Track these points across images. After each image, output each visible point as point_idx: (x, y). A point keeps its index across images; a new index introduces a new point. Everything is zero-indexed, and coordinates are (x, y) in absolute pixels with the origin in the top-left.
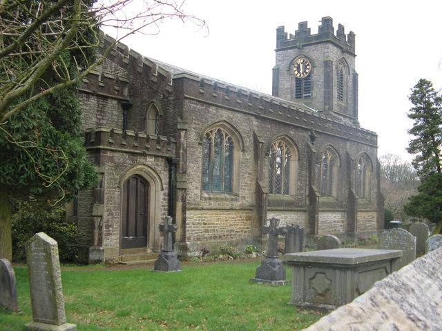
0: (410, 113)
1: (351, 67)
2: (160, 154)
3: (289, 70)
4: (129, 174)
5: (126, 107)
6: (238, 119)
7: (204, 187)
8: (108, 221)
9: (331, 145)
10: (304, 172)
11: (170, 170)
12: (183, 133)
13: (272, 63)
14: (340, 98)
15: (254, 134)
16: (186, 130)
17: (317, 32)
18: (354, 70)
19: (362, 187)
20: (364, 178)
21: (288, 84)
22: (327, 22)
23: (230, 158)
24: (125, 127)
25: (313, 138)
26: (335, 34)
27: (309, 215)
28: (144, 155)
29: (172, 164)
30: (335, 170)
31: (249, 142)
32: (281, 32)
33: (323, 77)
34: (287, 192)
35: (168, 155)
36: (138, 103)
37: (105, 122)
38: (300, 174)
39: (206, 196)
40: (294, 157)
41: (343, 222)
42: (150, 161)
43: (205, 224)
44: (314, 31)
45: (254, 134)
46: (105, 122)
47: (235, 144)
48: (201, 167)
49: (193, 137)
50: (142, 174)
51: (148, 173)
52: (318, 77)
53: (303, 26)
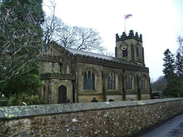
0: (164, 58)
1: (141, 46)
2: (70, 79)
3: (120, 48)
4: (60, 85)
5: (61, 64)
6: (95, 66)
7: (85, 88)
8: (53, 99)
9: (130, 73)
10: (121, 82)
11: (73, 84)
12: (77, 72)
13: (115, 46)
14: (138, 56)
15: (102, 71)
16: (78, 71)
17: (128, 35)
18: (142, 47)
19: (144, 86)
20: (145, 83)
21: (120, 52)
22: (131, 32)
23: (94, 79)
24: (61, 71)
25: (123, 71)
26: (135, 35)
27: (123, 96)
28: (65, 79)
29: (73, 81)
30: (133, 81)
31: (100, 74)
32: (117, 35)
33: (131, 50)
34: (115, 89)
35: (72, 79)
36: (64, 63)
37: (54, 69)
38: (119, 83)
39: (85, 91)
40: (117, 77)
41: (136, 98)
42: (66, 81)
43: (85, 100)
44: (128, 35)
45: (102, 71)
46: (54, 69)
47: (95, 74)
48: (83, 82)
49: (80, 73)
50: (64, 85)
51: (66, 85)
52: (129, 50)
53: (124, 33)
